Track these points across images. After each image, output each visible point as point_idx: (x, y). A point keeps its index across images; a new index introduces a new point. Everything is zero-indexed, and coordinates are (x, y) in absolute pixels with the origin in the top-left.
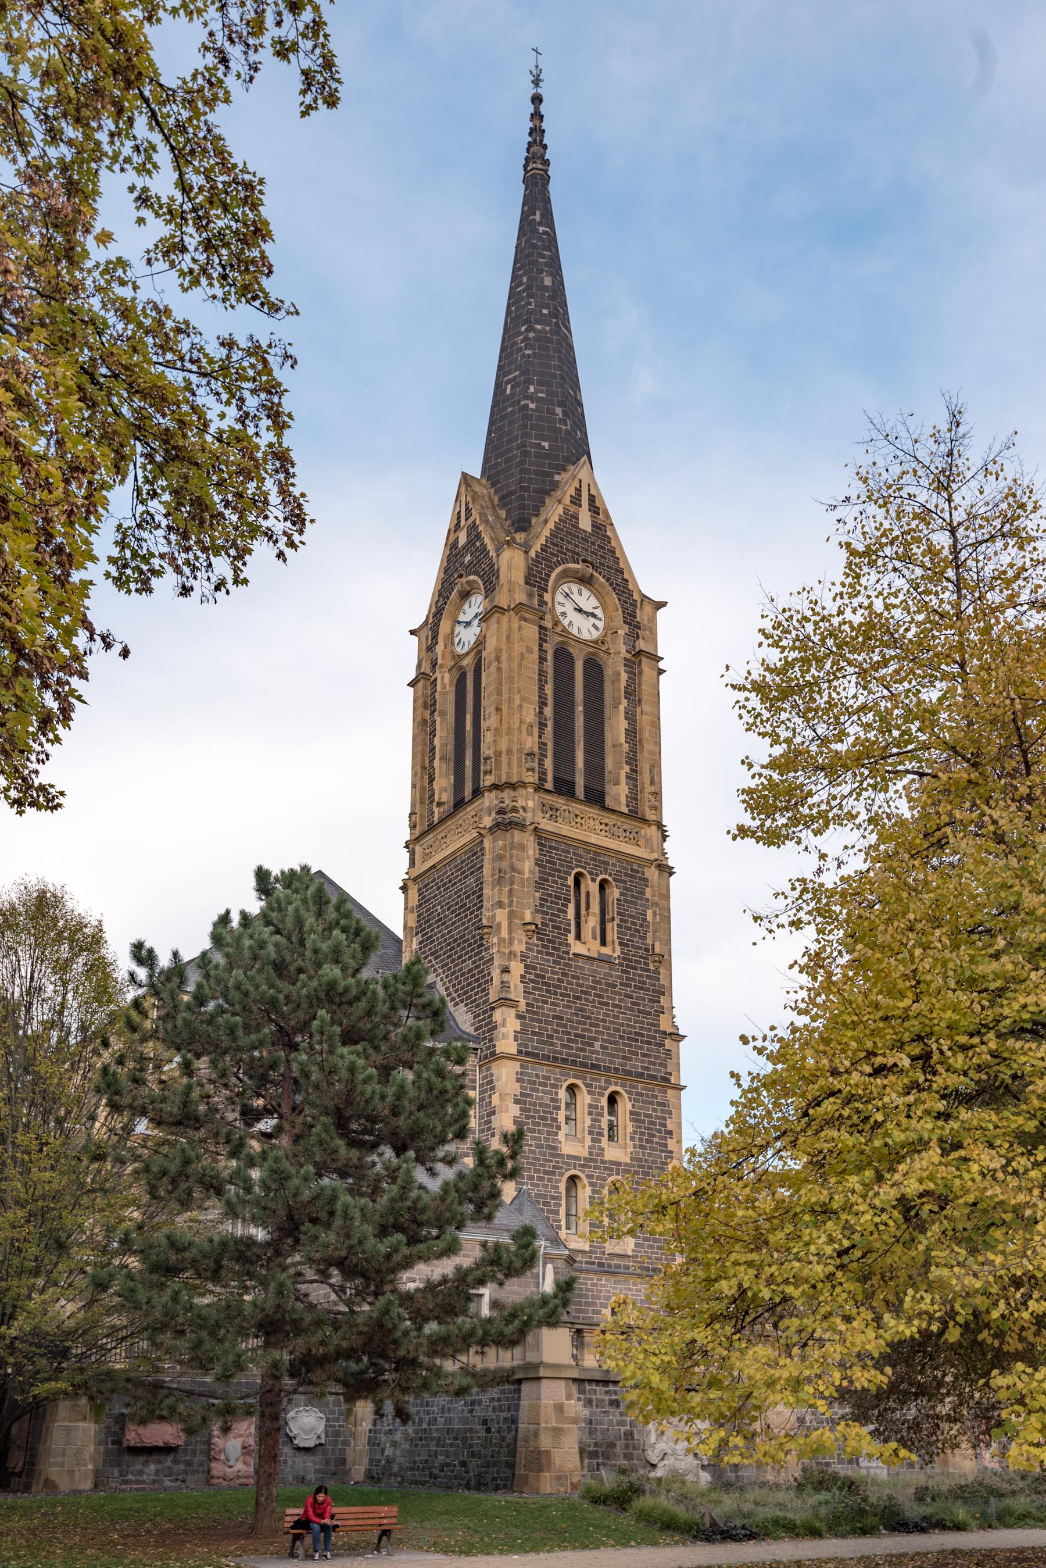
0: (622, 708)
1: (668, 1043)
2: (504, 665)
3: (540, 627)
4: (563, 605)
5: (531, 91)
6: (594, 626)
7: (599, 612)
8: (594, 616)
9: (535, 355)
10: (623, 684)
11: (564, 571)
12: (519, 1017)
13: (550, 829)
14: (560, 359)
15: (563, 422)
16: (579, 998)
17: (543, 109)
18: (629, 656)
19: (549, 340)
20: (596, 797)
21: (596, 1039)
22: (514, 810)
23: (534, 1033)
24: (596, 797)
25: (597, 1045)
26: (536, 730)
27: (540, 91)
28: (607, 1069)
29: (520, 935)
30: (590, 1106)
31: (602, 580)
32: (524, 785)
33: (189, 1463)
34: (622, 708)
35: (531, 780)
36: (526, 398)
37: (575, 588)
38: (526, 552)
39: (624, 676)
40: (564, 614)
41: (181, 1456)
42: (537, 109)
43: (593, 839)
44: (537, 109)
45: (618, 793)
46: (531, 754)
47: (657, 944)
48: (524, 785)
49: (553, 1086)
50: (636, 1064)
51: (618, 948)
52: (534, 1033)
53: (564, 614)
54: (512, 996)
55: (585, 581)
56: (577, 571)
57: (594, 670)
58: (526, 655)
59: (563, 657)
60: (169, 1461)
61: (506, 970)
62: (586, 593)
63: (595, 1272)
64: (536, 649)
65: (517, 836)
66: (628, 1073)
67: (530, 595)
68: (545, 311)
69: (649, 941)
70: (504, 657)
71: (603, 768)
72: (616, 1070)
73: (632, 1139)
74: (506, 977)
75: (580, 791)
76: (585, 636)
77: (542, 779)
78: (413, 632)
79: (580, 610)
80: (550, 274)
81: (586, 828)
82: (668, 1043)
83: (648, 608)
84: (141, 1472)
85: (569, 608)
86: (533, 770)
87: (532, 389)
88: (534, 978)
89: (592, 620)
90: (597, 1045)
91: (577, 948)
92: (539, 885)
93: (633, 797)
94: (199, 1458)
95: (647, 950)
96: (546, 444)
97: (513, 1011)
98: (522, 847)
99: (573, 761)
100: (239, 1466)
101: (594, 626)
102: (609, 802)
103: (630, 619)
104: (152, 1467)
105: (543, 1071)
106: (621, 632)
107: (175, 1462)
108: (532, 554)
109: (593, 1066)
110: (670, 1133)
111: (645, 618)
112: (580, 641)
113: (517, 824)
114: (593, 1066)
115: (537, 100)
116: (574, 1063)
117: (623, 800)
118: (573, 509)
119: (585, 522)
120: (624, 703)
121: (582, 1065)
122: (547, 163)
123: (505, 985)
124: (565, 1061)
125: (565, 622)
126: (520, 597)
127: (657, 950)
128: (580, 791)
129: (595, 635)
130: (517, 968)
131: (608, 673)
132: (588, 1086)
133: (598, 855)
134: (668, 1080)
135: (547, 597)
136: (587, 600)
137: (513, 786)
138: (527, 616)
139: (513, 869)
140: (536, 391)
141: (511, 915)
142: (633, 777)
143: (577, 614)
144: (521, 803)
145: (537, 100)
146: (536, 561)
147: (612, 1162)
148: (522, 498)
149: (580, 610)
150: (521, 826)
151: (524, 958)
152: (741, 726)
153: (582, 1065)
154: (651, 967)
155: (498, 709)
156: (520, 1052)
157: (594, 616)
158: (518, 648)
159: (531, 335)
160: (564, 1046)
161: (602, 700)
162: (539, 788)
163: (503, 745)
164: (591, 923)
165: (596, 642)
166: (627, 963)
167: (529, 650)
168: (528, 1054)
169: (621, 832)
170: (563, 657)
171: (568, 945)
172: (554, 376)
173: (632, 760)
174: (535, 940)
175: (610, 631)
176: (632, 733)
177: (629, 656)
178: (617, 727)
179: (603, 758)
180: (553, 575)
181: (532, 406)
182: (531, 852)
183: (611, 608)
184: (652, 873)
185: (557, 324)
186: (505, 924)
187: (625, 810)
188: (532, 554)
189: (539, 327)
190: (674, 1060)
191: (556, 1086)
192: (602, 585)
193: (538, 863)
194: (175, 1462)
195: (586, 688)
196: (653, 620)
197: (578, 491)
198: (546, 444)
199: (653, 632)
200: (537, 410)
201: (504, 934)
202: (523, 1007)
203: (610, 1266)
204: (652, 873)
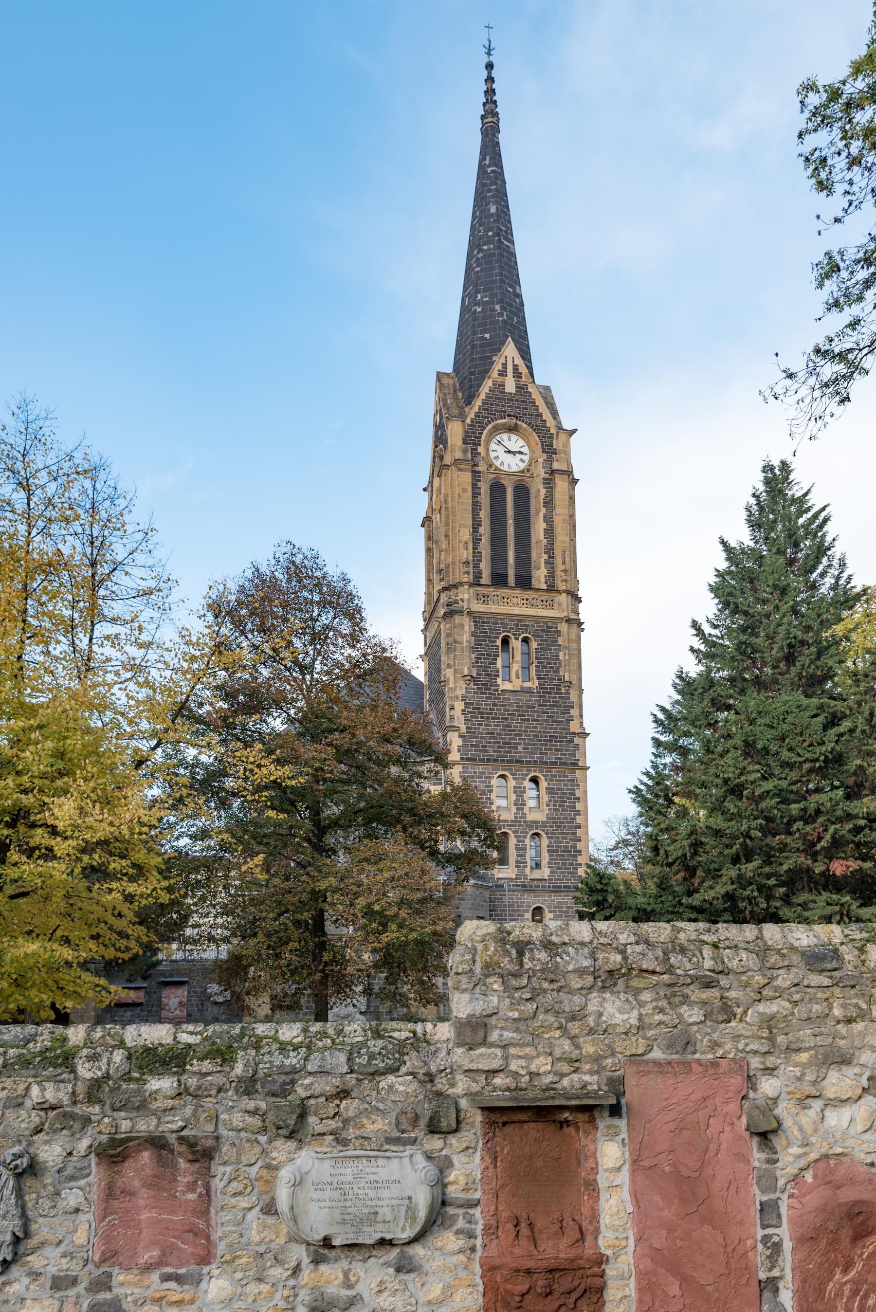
0: (541, 514)
1: (576, 740)
2: (450, 505)
3: (474, 472)
4: (496, 451)
5: (486, 59)
6: (522, 460)
7: (525, 450)
8: (521, 453)
9: (482, 270)
10: (542, 496)
11: (494, 427)
12: (460, 736)
13: (482, 610)
14: (501, 267)
15: (501, 315)
16: (506, 719)
17: (494, 74)
18: (547, 476)
19: (493, 255)
20: (524, 582)
21: (519, 744)
22: (456, 602)
23: (472, 746)
24: (524, 582)
25: (520, 748)
26: (470, 545)
27: (492, 59)
28: (529, 762)
29: (462, 684)
30: (515, 787)
31: (524, 425)
32: (461, 584)
33: (150, 1011)
34: (541, 514)
35: (466, 580)
36: (475, 305)
37: (505, 436)
38: (463, 421)
39: (543, 492)
40: (497, 458)
41: (145, 1008)
42: (490, 73)
43: (516, 611)
44: (490, 73)
45: (540, 576)
46: (467, 563)
47: (567, 675)
48: (461, 584)
49: (486, 777)
50: (551, 757)
51: (536, 682)
52: (472, 746)
53: (497, 458)
54: (456, 724)
55: (512, 429)
56: (505, 424)
57: (522, 492)
58: (463, 495)
59: (497, 489)
60: (138, 1010)
61: (452, 708)
62: (514, 437)
63: (519, 891)
64: (470, 488)
65: (457, 619)
66: (545, 763)
67: (465, 452)
68: (490, 234)
69: (561, 673)
70: (450, 500)
71: (530, 559)
72: (535, 762)
73: (548, 805)
74: (452, 713)
75: (511, 580)
76: (514, 469)
77: (478, 576)
78: (425, 490)
79: (509, 452)
80: (497, 203)
81: (513, 604)
82: (576, 740)
83: (563, 437)
84: (122, 1016)
85: (501, 450)
86: (468, 573)
87: (479, 296)
88: (473, 711)
89: (518, 456)
90: (520, 748)
91: (507, 686)
92: (474, 649)
93: (551, 576)
94: (155, 1008)
95: (559, 680)
96: (487, 336)
97: (456, 734)
98: (462, 626)
99: (506, 560)
100: (178, 1012)
101: (522, 460)
102: (535, 583)
103: (549, 450)
104: (129, 1013)
105: (479, 769)
106: (541, 460)
107: (142, 1010)
108: (468, 421)
109: (517, 761)
110: (578, 798)
111: (561, 445)
112: (508, 474)
113: (456, 611)
114: (517, 761)
115: (490, 66)
116: (503, 761)
117: (543, 580)
118: (500, 379)
119: (510, 387)
120: (544, 510)
121: (508, 761)
122: (497, 114)
123: (452, 718)
124: (495, 761)
125: (497, 463)
126: (459, 455)
127: (567, 679)
128: (511, 580)
129: (522, 466)
130: (459, 706)
131: (533, 491)
132: (512, 774)
133: (520, 622)
134: (576, 764)
135: (480, 449)
136: (514, 442)
137: (455, 586)
138: (462, 467)
139: (455, 642)
140: (482, 297)
141: (456, 672)
142: (550, 562)
143: (508, 455)
144: (461, 596)
145: (490, 66)
146: (471, 426)
147: (532, 822)
148: (470, 380)
149: (509, 452)
150: (460, 612)
151: (464, 698)
152: (323, 556)
153: (508, 761)
154: (563, 690)
155: (446, 536)
156: (462, 759)
157: (521, 453)
158: (457, 491)
159: (480, 255)
160: (495, 751)
161: (529, 511)
162: (476, 583)
163: (450, 559)
164: (516, 667)
165: (523, 472)
166: (543, 691)
167: (464, 490)
168: (468, 759)
169: (539, 603)
170: (497, 489)
171: (498, 685)
172: (495, 282)
173: (550, 550)
174: (472, 686)
175: (533, 461)
176: (550, 532)
177: (547, 476)
178: (539, 528)
179: (530, 553)
180: (485, 432)
181: (479, 310)
182: (467, 628)
183: (533, 444)
184: (563, 627)
185: (500, 241)
186: (452, 678)
187: (544, 586)
188: (468, 421)
189: (485, 247)
190: (581, 751)
191: (490, 778)
192: (525, 429)
193: (474, 634)
194: (142, 1010)
195: (516, 506)
196: (567, 445)
197: (505, 365)
198: (487, 336)
199: (567, 454)
200: (482, 312)
201: (451, 685)
202: (463, 729)
203: (531, 886)
204: (563, 627)
